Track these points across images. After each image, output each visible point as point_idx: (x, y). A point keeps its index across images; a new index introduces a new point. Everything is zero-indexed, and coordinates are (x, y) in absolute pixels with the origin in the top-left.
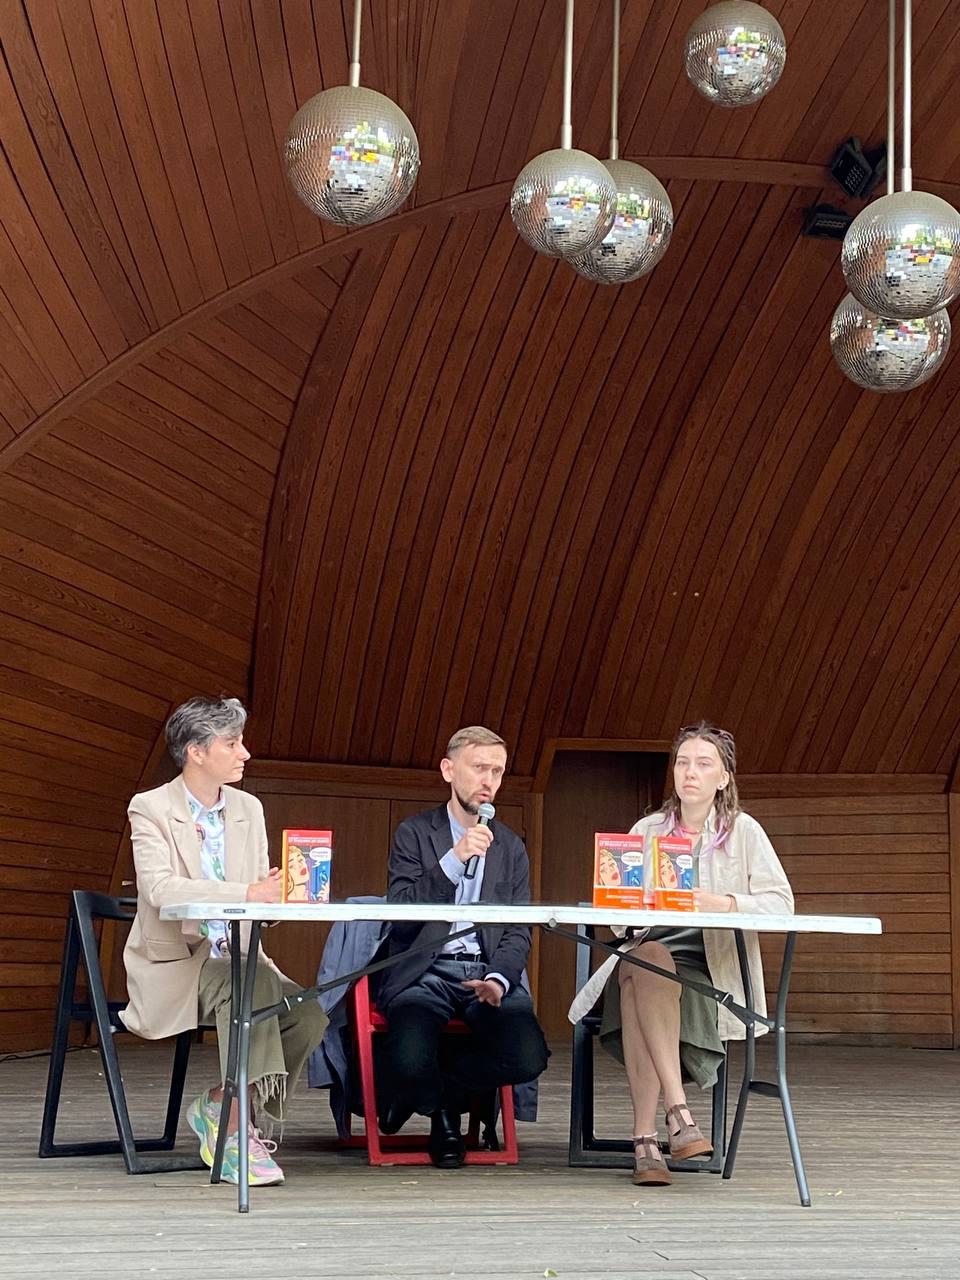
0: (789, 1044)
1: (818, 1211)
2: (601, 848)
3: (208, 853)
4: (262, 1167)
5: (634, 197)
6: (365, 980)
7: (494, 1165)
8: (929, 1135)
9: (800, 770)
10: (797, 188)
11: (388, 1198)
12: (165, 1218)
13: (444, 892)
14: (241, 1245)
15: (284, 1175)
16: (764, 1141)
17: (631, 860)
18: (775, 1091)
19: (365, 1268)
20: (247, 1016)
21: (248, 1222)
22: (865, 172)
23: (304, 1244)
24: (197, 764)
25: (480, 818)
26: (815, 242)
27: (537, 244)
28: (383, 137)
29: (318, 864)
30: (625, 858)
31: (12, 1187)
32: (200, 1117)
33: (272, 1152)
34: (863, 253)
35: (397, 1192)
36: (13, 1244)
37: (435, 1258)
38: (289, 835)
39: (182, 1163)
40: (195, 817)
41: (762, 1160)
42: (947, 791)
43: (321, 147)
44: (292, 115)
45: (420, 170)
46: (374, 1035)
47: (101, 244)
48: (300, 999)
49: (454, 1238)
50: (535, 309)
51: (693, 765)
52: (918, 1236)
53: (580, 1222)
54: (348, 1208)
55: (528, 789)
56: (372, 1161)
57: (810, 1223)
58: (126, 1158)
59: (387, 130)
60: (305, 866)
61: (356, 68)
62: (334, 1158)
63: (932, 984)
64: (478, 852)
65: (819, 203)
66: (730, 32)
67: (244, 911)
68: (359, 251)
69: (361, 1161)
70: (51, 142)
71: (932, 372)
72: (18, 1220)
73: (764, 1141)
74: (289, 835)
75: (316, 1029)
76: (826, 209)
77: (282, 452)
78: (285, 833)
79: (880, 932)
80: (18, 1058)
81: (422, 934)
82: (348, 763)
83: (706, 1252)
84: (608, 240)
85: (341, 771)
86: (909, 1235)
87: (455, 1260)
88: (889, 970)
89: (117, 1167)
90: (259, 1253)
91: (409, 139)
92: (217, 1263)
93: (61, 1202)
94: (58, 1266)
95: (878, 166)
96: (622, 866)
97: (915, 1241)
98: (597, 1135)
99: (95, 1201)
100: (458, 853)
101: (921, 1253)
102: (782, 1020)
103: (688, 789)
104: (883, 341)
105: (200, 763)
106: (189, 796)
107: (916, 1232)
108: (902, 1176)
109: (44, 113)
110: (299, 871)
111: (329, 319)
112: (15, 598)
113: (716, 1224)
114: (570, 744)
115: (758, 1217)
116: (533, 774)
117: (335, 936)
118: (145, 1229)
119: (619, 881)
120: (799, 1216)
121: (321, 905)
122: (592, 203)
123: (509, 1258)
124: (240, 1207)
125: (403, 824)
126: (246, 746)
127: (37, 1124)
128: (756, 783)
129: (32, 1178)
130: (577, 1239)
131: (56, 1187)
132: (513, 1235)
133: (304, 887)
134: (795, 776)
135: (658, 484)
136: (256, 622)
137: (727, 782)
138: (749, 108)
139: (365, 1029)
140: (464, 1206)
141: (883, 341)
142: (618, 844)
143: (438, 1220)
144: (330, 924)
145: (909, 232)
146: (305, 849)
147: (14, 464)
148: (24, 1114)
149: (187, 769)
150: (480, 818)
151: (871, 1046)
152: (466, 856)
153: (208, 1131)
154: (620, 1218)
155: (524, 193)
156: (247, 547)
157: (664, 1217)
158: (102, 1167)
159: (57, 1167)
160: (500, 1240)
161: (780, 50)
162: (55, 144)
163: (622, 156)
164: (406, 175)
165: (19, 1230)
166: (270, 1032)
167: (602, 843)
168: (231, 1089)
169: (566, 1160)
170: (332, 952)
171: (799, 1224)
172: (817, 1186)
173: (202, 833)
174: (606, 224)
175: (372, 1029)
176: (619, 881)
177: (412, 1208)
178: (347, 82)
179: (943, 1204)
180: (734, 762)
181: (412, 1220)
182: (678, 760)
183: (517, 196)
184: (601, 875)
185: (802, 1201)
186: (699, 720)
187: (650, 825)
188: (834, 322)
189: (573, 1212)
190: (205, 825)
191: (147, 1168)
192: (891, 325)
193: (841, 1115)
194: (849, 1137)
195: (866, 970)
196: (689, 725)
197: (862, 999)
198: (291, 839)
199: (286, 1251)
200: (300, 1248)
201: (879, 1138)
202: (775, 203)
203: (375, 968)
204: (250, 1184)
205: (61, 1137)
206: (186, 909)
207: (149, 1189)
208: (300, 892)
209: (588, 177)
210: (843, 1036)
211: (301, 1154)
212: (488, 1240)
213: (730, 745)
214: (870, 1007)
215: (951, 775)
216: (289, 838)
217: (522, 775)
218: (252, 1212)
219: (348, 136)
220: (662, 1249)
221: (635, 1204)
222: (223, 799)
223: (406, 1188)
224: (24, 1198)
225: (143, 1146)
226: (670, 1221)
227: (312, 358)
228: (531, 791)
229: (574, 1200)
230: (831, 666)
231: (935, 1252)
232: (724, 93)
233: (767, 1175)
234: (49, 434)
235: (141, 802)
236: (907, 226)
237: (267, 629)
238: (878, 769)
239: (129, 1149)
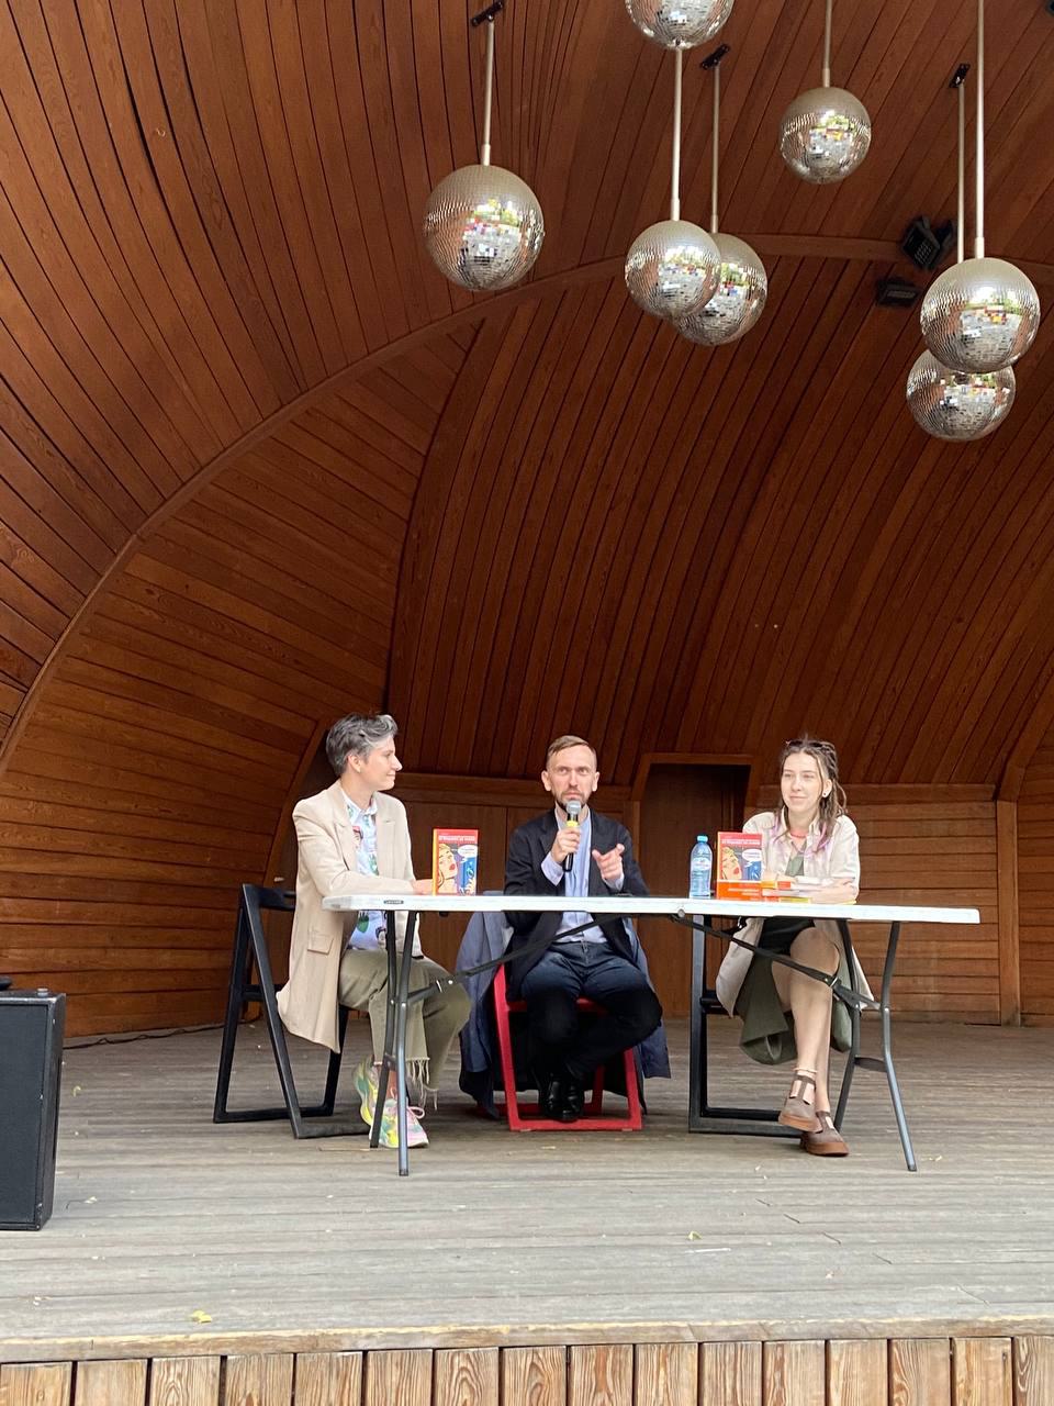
0: (892, 1020)
2: (723, 846)
4: (403, 1128)
6: (503, 967)
7: (620, 1130)
8: (1003, 1103)
9: (864, 781)
10: (871, 262)
17: (750, 856)
18: (882, 1067)
19: (522, 1230)
20: (403, 997)
21: (408, 1185)
22: (931, 245)
24: (355, 771)
26: (888, 311)
27: (650, 307)
28: (513, 211)
29: (465, 860)
30: (461, 851)
32: (363, 1083)
33: (420, 1117)
34: (940, 313)
36: (198, 1205)
37: (585, 1220)
39: (342, 1129)
40: (353, 820)
41: (860, 1127)
42: (996, 797)
44: (428, 196)
45: (544, 240)
48: (450, 982)
50: (636, 373)
51: (798, 777)
52: (1022, 1200)
53: (711, 1185)
56: (513, 1128)
57: (920, 1188)
58: (292, 1123)
60: (454, 862)
61: (487, 148)
62: (477, 1124)
63: (981, 968)
65: (890, 277)
66: (819, 115)
67: (402, 902)
68: (483, 321)
69: (503, 1127)
70: (215, 218)
71: (1000, 422)
75: (461, 1011)
76: (897, 281)
78: (435, 831)
79: (978, 922)
80: (186, 1032)
82: (470, 774)
83: (832, 1216)
84: (713, 304)
85: (469, 783)
87: (604, 1223)
89: (284, 1132)
90: (423, 1215)
91: (534, 215)
92: (385, 1225)
94: (241, 1227)
95: (946, 241)
96: (743, 862)
97: (1021, 1204)
98: (711, 1104)
101: (1030, 1217)
102: (887, 1002)
103: (795, 800)
104: (956, 395)
105: (358, 770)
106: (348, 801)
108: (990, 1142)
109: (209, 190)
110: (448, 866)
112: (181, 629)
113: (835, 1188)
114: (663, 758)
115: (872, 1181)
116: (631, 784)
117: (473, 927)
120: (905, 1180)
122: (694, 268)
123: (653, 1221)
124: (400, 1171)
125: (517, 831)
126: (398, 758)
127: (212, 1092)
128: (861, 785)
129: (210, 1142)
130: (712, 1202)
131: (232, 1151)
133: (453, 880)
134: (862, 786)
138: (832, 185)
141: (956, 395)
142: (739, 842)
143: (581, 1184)
144: (470, 913)
146: (454, 846)
149: (345, 776)
153: (369, 1092)
154: (745, 1181)
155: (636, 260)
156: (382, 585)
157: (787, 1181)
158: (270, 1132)
161: (866, 132)
163: (720, 230)
165: (202, 1192)
166: (417, 1012)
168: (389, 1063)
170: (470, 944)
171: (911, 1187)
172: (922, 1151)
174: (711, 288)
176: (740, 875)
178: (479, 161)
180: (836, 770)
181: (558, 1183)
184: (724, 870)
185: (909, 1167)
188: (910, 379)
189: (701, 1175)
192: (961, 380)
193: (920, 1084)
194: (932, 1105)
196: (792, 738)
197: (920, 982)
198: (440, 838)
200: (461, 1210)
202: (859, 271)
203: (508, 958)
205: (232, 1105)
206: (349, 900)
207: (315, 1153)
208: (450, 886)
209: (695, 245)
210: (931, 1017)
211: (466, 1114)
212: (628, 1204)
213: (832, 755)
215: (999, 786)
216: (440, 837)
218: (412, 1176)
220: (793, 1212)
221: (757, 1169)
222: (375, 805)
223: (546, 1152)
225: (307, 1113)
228: (629, 799)
232: (815, 171)
234: (212, 483)
235: (303, 807)
239: (295, 1116)
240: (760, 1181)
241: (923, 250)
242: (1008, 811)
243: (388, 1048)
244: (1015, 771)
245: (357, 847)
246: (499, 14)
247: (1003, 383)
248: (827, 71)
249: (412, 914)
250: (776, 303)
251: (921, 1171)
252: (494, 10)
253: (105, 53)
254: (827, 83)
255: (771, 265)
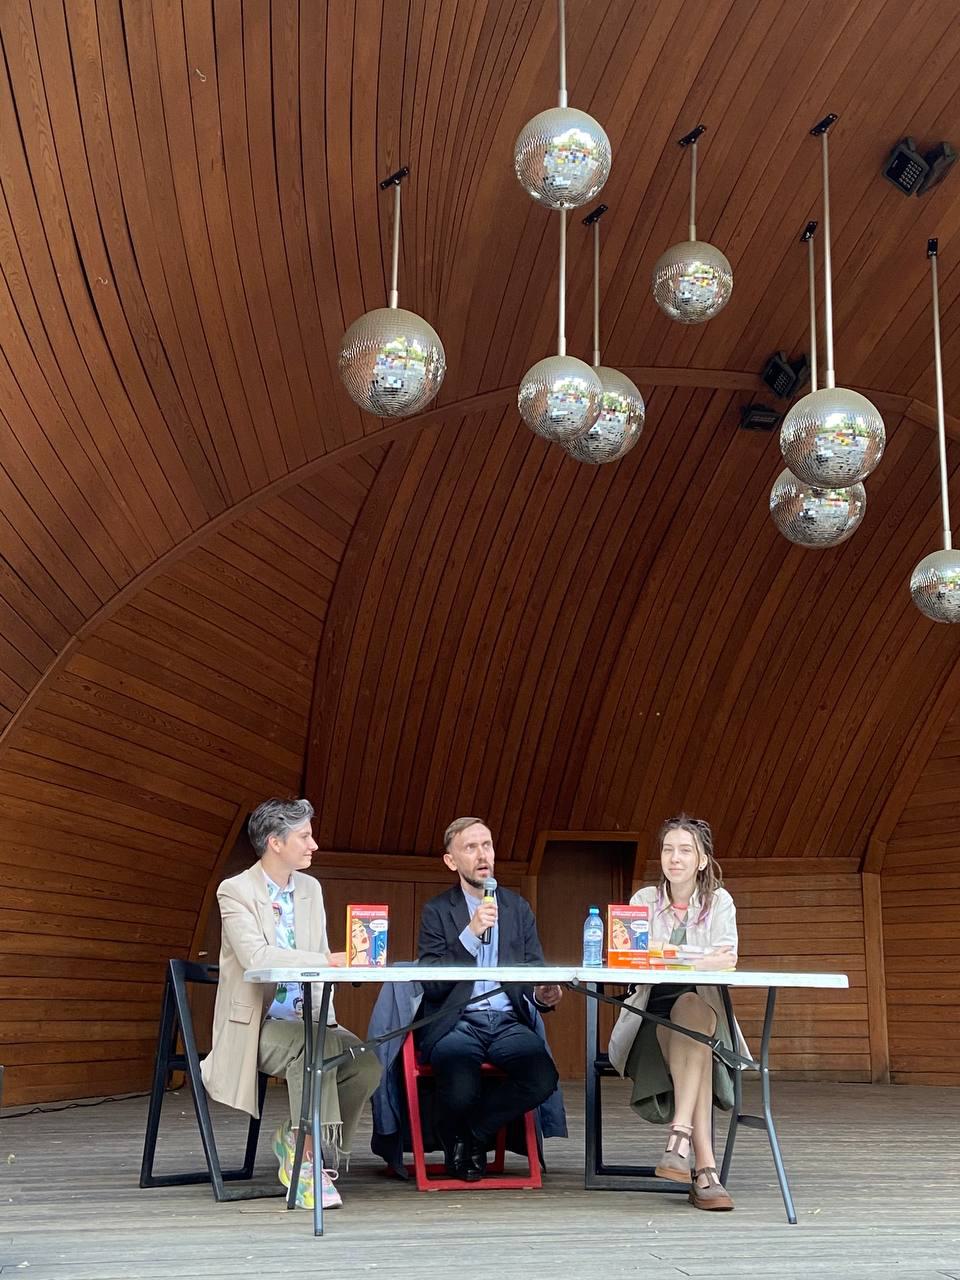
1: (803, 1228)
2: (613, 917)
3: (277, 924)
4: (318, 1190)
5: (614, 395)
7: (521, 1189)
10: (735, 392)
11: (439, 1221)
12: (253, 1243)
13: (466, 959)
14: (321, 1266)
15: (342, 1199)
16: (741, 1164)
17: (639, 927)
18: (762, 1124)
20: (319, 1064)
22: (789, 377)
23: (374, 1265)
25: (486, 891)
31: (118, 1215)
34: (798, 437)
35: (445, 1216)
36: (124, 1268)
38: (352, 910)
39: (261, 1191)
41: (743, 1181)
42: (860, 870)
43: (368, 355)
45: (446, 374)
46: (418, 1078)
47: (189, 436)
48: (363, 1049)
49: (502, 1257)
50: (530, 487)
51: (676, 851)
52: (895, 1250)
53: (606, 1241)
54: (406, 1230)
55: (524, 872)
56: (421, 1188)
57: (801, 1240)
59: (420, 342)
61: (395, 294)
63: (852, 1029)
64: (491, 924)
66: (687, 265)
67: (318, 974)
68: (392, 442)
69: (410, 1187)
71: (852, 531)
72: (127, 1246)
73: (741, 1164)
74: (352, 910)
76: (759, 408)
77: (329, 602)
78: (349, 908)
81: (455, 991)
82: (381, 852)
85: (377, 858)
86: (888, 1250)
88: (817, 1018)
89: (205, 1195)
93: (161, 1228)
96: (631, 932)
98: (606, 1162)
99: (191, 1227)
100: (475, 929)
102: (766, 1062)
104: (813, 507)
105: (278, 851)
107: (893, 1246)
108: (864, 1195)
109: (146, 331)
111: (366, 497)
114: (560, 835)
116: (529, 860)
118: (237, 1253)
119: (629, 945)
120: (784, 1233)
121: (379, 969)
122: (581, 397)
128: (731, 860)
129: (136, 1206)
132: (553, 1254)
134: (738, 860)
135: (626, 628)
136: (307, 740)
137: (706, 863)
139: (411, 1073)
140: (504, 1227)
141: (813, 507)
142: (627, 914)
144: (381, 984)
145: (834, 420)
146: (366, 921)
147: (116, 613)
148: (123, 1149)
149: (268, 857)
150: (486, 891)
151: (805, 1081)
152: (481, 930)
155: (528, 390)
156: (300, 679)
158: (192, 1196)
159: (157, 1197)
160: (543, 1258)
161: (728, 279)
162: (155, 356)
164: (435, 376)
166: (332, 1077)
167: (614, 913)
169: (582, 1184)
173: (278, 910)
175: (416, 1073)
176: (629, 945)
177: (461, 1229)
178: (388, 305)
179: (907, 1220)
180: (711, 846)
182: (665, 847)
183: (524, 392)
185: (790, 1220)
186: (680, 814)
187: (644, 896)
190: (281, 903)
191: (232, 1197)
195: (799, 1018)
197: (797, 1042)
199: (359, 1272)
201: (835, 1160)
204: (324, 1206)
205: (159, 1169)
206: (269, 973)
208: (362, 958)
210: (797, 1075)
212: (530, 1259)
213: (707, 832)
214: (803, 1049)
216: (353, 912)
217: (519, 861)
218: (327, 1235)
219: (389, 346)
221: (649, 1223)
224: (130, 1225)
225: (228, 1176)
226: (681, 1239)
227: (353, 528)
229: (595, 1220)
230: (766, 771)
231: (914, 1265)
232: (685, 313)
233: (751, 1196)
236: (833, 415)
237: (316, 745)
238: (806, 852)
239: (217, 1180)
240: (651, 1235)
241: (781, 379)
242: (871, 879)
243: (305, 1113)
244: (878, 847)
245: (277, 924)
246: (405, 179)
247: (855, 497)
248: (693, 228)
249: (327, 985)
250: (653, 428)
251: (801, 1223)
252: (400, 175)
253: (55, 214)
254: (693, 238)
255: (649, 395)
